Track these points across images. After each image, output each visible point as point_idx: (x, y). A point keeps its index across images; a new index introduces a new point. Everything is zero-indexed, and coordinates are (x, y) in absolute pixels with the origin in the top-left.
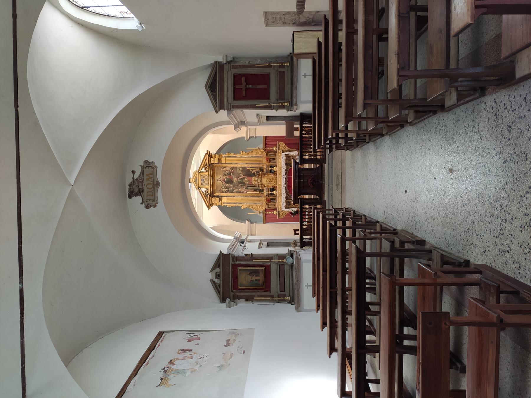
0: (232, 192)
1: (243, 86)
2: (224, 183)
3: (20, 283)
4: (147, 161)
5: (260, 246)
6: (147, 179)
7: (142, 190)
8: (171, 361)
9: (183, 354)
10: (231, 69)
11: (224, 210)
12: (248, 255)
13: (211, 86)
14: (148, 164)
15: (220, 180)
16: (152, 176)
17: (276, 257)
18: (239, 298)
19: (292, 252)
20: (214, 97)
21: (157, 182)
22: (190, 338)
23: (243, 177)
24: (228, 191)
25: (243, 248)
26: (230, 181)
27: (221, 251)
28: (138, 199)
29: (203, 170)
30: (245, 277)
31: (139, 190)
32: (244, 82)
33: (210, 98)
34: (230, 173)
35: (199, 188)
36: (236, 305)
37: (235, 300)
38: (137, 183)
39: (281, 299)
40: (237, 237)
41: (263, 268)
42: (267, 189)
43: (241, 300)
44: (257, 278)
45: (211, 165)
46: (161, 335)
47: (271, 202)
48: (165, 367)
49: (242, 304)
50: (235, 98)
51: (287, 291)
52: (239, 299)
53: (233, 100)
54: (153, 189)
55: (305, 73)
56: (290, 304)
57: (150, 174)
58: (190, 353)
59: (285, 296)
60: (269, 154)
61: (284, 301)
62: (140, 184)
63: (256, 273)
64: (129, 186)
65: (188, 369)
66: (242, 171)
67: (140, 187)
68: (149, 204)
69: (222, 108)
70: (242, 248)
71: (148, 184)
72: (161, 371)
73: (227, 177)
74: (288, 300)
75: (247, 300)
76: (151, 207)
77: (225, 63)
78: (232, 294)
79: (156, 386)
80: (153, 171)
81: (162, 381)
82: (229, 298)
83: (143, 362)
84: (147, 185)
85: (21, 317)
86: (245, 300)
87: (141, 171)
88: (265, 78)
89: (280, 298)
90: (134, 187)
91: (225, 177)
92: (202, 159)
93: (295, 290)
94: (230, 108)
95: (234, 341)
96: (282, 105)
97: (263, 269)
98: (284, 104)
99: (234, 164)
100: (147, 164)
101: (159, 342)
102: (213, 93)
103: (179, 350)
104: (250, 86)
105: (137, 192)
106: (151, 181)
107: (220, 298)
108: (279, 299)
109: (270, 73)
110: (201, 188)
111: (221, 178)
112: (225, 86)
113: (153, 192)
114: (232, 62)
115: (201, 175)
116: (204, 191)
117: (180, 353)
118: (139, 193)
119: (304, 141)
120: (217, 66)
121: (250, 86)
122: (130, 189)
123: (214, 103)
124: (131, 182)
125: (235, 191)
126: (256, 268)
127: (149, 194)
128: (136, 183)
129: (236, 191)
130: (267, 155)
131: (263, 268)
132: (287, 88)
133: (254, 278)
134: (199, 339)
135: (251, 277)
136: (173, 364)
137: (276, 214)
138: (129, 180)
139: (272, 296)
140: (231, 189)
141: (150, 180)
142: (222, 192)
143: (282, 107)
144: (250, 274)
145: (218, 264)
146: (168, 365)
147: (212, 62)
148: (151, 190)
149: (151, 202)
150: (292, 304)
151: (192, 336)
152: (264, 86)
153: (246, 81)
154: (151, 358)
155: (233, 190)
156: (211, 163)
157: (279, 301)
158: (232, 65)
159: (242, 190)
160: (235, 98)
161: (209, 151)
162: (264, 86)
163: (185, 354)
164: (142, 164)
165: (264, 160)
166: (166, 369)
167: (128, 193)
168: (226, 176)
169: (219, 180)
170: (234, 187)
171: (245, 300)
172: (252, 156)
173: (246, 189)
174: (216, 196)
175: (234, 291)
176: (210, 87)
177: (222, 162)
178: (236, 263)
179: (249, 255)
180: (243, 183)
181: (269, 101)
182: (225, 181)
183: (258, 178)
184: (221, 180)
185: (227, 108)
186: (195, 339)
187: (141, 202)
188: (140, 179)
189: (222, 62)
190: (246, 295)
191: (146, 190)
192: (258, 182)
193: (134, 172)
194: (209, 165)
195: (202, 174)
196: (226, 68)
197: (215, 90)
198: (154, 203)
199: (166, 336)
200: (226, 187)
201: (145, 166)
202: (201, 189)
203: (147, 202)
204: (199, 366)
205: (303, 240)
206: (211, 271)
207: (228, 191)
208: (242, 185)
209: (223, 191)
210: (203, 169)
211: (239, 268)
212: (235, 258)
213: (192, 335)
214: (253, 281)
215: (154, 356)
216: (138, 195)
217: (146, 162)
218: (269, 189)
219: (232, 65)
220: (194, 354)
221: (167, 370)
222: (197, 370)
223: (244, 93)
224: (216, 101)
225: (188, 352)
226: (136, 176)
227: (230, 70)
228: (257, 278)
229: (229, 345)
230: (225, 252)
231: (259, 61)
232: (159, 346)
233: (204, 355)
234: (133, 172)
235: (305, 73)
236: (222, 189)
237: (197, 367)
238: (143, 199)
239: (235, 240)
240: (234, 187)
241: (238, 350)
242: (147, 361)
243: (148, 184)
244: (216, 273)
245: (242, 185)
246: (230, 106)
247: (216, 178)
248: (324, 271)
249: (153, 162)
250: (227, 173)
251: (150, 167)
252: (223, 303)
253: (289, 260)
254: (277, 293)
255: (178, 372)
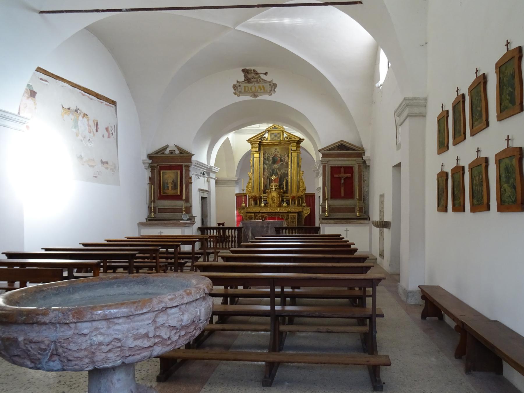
0: (264, 163)
1: (343, 175)
2: (273, 156)
3: (126, 9)
4: (276, 86)
5: (201, 190)
6: (259, 87)
7: (250, 82)
8: (86, 115)
9: (94, 124)
10: (358, 164)
11: (248, 155)
12: (190, 179)
13: (343, 146)
14: (274, 87)
15: (275, 152)
16: (263, 91)
17: (188, 205)
18: (152, 172)
19: (193, 220)
20: (333, 148)
21: (257, 95)
22: (110, 129)
23: (279, 174)
24: (265, 159)
25: (199, 175)
26: (274, 161)
27: (194, 154)
28: (241, 77)
29: (285, 135)
30: (171, 177)
31: (250, 79)
32: (346, 175)
33: (332, 145)
34: (283, 162)
35: (268, 131)
36: (146, 169)
37: (150, 168)
38: (256, 77)
39: (152, 210)
40: (212, 169)
41: (179, 194)
42: (266, 197)
43: (150, 173)
44: (170, 188)
45: (289, 143)
46: (113, 103)
47: (254, 201)
48: (80, 110)
49: (147, 174)
50: (332, 168)
51: (159, 215)
52: (151, 171)
53: (331, 166)
54: (251, 92)
55: (349, 230)
56: (147, 218)
57: (264, 89)
58: (95, 131)
59: (155, 213)
60: (300, 199)
61: (150, 212)
62: (255, 80)
63: (175, 187)
64: (253, 70)
65: (78, 130)
66: (284, 173)
67: (252, 80)
68: (237, 89)
69: (324, 155)
70: (199, 174)
71: (255, 87)
72: (76, 107)
73: (279, 159)
74: (151, 215)
75: (150, 178)
76: (234, 90)
77: (364, 158)
78: (155, 165)
79: (62, 105)
80: (267, 92)
81: (67, 109)
82: (152, 163)
83: (85, 91)
84: (254, 86)
85: (101, 10)
86: (150, 176)
87: (267, 81)
88: (350, 195)
89: (153, 208)
90: (253, 75)
91: (279, 156)
92: (295, 135)
93: (156, 222)
94: (324, 163)
95: (107, 168)
96: (326, 211)
97: (178, 193)
98: (326, 212)
99: (291, 165)
100: (273, 86)
101: (105, 103)
102: (337, 147)
103: (97, 120)
104: (343, 181)
105: (248, 77)
106: (258, 90)
107: (151, 154)
108: (152, 208)
109: (354, 199)
110: (268, 133)
111: (278, 152)
112: (343, 159)
113: (248, 92)
114: (365, 165)
115: (280, 133)
116: (265, 136)
117: (94, 122)
118: (247, 79)
119: (286, 231)
120: (361, 152)
121: (343, 181)
122: (251, 70)
123: (328, 148)
124: (257, 72)
125: (265, 166)
126: (179, 187)
127: (247, 88)
128: (256, 76)
129: (265, 167)
130: (299, 197)
131: (179, 194)
132: (340, 215)
133: (170, 185)
134: (109, 137)
135: (171, 182)
136: (83, 117)
137: (242, 206)
138: (259, 70)
139: (154, 201)
140: (267, 162)
141: (259, 89)
142: (264, 153)
143: (324, 211)
144: (173, 181)
145: (182, 152)
146: (83, 113)
147: (365, 147)
148: (250, 90)
149: (239, 90)
150: (146, 219)
151: (111, 131)
152: (342, 195)
153: (347, 177)
154: (89, 97)
155: (266, 164)
156: (291, 143)
157: (150, 208)
158: (361, 165)
159: (266, 173)
160: (332, 168)
161: (304, 141)
162: (342, 195)
163: (94, 126)
164: (274, 82)
165: (294, 194)
166: (79, 111)
167: (247, 69)
168: (280, 157)
169: (276, 151)
170: (270, 165)
171: (150, 176)
172: (298, 183)
173: (267, 176)
174: (260, 148)
175: (159, 167)
176: (342, 145)
177: (292, 154)
178: (184, 168)
179: (191, 180)
180: (273, 173)
181: (330, 198)
182: (274, 156)
183: (277, 188)
184: (276, 153)
185: (323, 160)
186: (109, 134)
187: (239, 81)
188: (260, 80)
189: (364, 156)
190: (155, 178)
191: (250, 85)
192: (272, 188)
193: (266, 74)
194: (289, 141)
195: (282, 134)
196: (360, 159)
197: (340, 150)
198: (237, 93)
199: (112, 108)
200: (269, 157)
201: (272, 84)
202: (267, 133)
203: (239, 86)
204: (82, 139)
205: (206, 230)
206: (175, 146)
207: (265, 159)
208: (271, 173)
209: (265, 154)
210: (287, 136)
211: (179, 172)
212: (188, 167)
213: (112, 130)
214: (167, 183)
215: (91, 99)
216: (245, 78)
217: (275, 86)
218: (266, 199)
219: (361, 165)
220: (93, 134)
221: (78, 112)
222: (78, 138)
223: (337, 176)
224: (329, 150)
225: (96, 128)
226: (263, 76)
227: (357, 163)
228: (170, 188)
229: (102, 164)
230: (194, 158)
231: (367, 190)
232: (102, 103)
233: (93, 142)
234: (266, 74)
235: (349, 230)
236: (267, 153)
237: (80, 137)
238: (242, 83)
239: (209, 167)
240: (270, 165)
241: (97, 171)
242: (86, 94)
243: (255, 87)
244: (174, 150)
245: (271, 173)
246: (325, 163)
247: (277, 147)
248: (152, 241)
249: (275, 92)
250: (283, 159)
251: (270, 89)
252: (148, 157)
253: (185, 217)
254: (157, 206)
255: (76, 121)
